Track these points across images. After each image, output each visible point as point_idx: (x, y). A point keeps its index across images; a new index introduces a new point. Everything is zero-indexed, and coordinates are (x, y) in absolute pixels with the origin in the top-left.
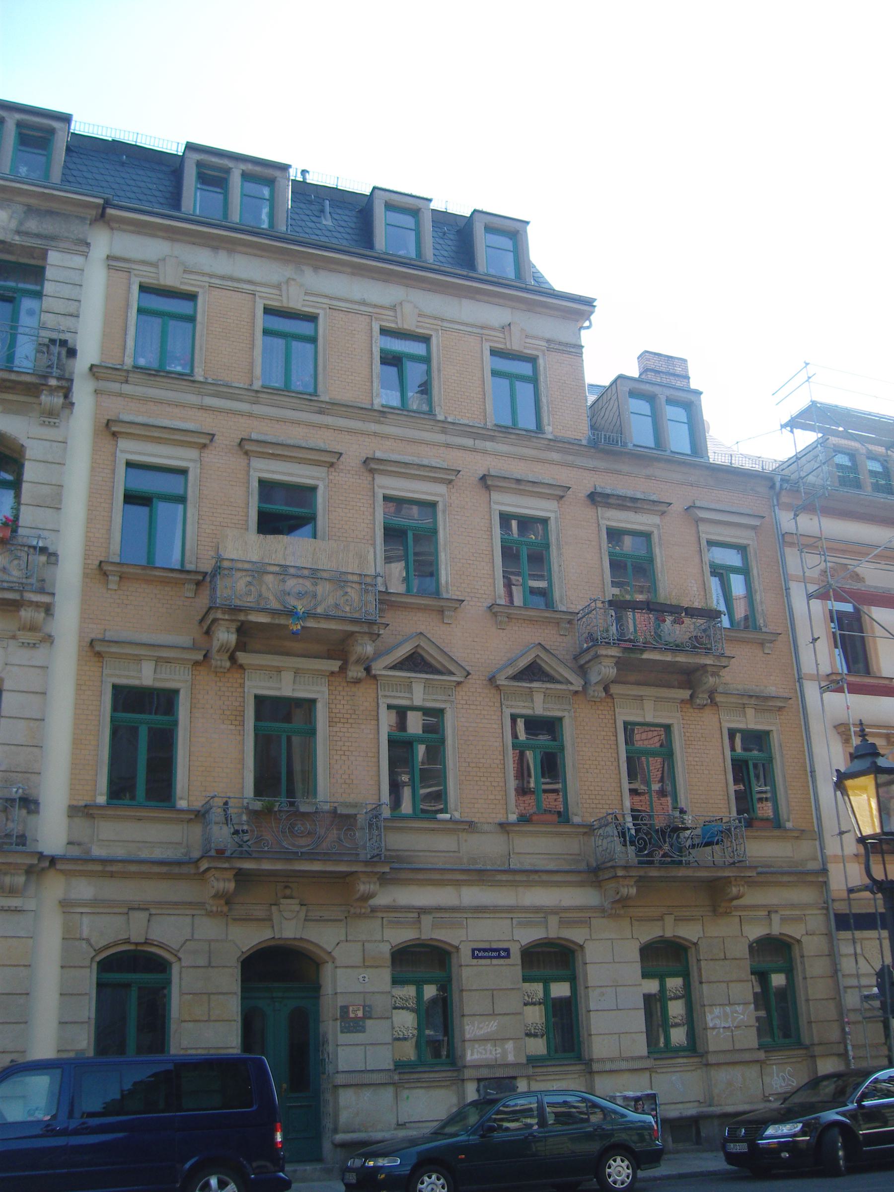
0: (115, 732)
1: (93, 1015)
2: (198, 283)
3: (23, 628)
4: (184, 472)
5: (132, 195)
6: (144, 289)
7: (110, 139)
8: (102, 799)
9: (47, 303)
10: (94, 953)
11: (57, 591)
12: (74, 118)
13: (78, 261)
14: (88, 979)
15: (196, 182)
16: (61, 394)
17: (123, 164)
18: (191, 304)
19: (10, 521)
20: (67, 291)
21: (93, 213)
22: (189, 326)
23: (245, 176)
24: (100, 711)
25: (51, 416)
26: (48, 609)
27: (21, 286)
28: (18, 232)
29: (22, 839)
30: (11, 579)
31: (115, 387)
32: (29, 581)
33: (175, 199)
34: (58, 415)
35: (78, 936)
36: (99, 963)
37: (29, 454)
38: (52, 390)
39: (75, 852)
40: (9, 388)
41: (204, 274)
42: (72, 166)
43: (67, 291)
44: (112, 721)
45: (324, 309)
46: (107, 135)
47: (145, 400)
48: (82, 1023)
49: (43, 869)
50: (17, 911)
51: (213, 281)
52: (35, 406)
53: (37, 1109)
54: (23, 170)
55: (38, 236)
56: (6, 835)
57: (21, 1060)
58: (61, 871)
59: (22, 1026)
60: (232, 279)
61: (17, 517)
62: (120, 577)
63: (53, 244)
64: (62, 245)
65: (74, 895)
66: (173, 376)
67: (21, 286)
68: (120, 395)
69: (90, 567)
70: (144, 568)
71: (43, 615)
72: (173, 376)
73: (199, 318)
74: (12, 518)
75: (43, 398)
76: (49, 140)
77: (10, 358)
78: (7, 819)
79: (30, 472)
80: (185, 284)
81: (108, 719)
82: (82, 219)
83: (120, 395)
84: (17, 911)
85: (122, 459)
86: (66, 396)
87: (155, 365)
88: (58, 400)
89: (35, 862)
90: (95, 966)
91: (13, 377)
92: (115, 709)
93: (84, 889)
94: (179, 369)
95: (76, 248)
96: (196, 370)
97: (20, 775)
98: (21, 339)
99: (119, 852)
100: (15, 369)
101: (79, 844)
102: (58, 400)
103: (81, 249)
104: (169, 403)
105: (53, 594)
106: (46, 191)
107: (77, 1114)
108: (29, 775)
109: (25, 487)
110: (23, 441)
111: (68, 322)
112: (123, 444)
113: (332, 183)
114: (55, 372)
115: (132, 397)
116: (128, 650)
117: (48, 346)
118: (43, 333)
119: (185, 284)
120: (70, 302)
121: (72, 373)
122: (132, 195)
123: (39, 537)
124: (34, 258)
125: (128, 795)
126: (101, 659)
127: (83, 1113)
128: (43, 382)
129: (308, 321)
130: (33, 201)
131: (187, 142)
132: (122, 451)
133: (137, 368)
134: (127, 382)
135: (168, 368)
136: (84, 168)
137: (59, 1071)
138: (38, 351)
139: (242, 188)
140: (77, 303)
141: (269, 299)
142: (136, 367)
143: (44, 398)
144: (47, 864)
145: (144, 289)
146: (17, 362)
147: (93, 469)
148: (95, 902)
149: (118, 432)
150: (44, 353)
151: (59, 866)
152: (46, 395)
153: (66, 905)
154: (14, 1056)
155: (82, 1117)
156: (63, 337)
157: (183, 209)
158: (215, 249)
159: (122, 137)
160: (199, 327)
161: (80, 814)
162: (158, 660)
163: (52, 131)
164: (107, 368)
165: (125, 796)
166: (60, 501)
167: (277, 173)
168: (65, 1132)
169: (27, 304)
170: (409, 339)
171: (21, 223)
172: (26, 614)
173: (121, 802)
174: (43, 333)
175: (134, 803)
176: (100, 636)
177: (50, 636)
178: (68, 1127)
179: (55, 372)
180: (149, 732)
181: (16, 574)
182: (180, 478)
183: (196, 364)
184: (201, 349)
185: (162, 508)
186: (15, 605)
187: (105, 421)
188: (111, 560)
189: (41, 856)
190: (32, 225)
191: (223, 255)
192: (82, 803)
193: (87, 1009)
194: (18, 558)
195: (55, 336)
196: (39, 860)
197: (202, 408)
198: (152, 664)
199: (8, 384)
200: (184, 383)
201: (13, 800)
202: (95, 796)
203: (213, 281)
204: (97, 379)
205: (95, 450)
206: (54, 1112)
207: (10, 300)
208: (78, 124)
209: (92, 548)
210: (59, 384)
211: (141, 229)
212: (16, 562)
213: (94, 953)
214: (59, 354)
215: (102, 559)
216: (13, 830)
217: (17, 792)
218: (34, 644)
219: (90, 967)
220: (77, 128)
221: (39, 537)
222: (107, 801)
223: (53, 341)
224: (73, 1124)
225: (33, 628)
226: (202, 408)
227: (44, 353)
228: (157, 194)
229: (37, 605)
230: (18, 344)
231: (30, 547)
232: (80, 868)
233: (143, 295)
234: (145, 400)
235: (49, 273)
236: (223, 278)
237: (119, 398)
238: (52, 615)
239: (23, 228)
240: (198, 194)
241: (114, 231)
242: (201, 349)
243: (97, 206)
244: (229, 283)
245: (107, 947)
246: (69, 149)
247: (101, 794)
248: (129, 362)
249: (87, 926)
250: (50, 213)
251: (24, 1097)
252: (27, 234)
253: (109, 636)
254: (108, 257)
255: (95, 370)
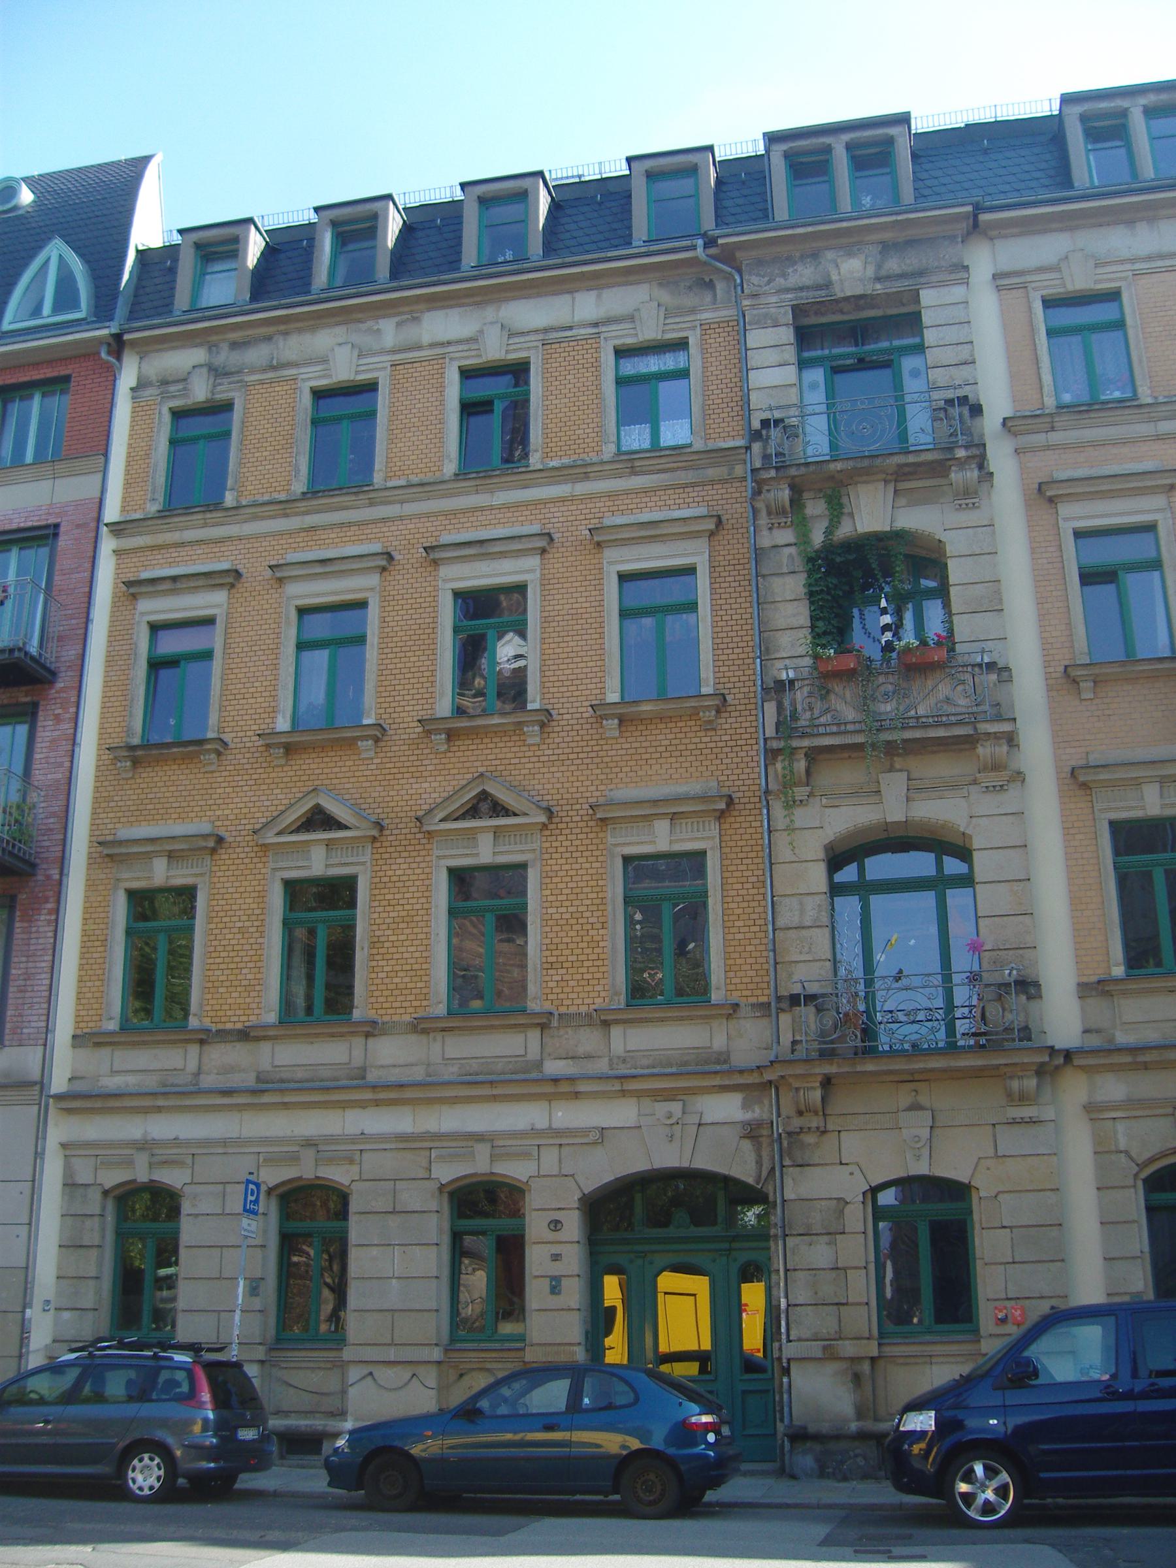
0: (1123, 880)
1: (1147, 1249)
2: (1118, 275)
3: (983, 769)
4: (1150, 528)
5: (1007, 188)
6: (1048, 303)
7: (962, 125)
8: (1119, 971)
9: (932, 356)
10: (1136, 1169)
11: (1017, 716)
12: (913, 116)
13: (958, 292)
14: (1134, 1203)
15: (1086, 144)
16: (973, 466)
17: (986, 152)
18: (1115, 305)
19: (945, 638)
20: (951, 334)
21: (964, 226)
22: (1117, 335)
23: (1150, 113)
24: (1098, 858)
25: (968, 497)
26: (1011, 739)
27: (897, 343)
28: (878, 279)
29: (1026, 1033)
30: (959, 710)
31: (1040, 439)
32: (980, 708)
33: (1063, 175)
34: (976, 493)
35: (1113, 1148)
36: (1145, 1181)
37: (949, 550)
38: (962, 463)
39: (1094, 1041)
40: (909, 473)
41: (1122, 262)
42: (924, 175)
43: (951, 334)
44: (1115, 868)
45: (1125, 279)
46: (957, 121)
47: (1080, 446)
48: (1134, 1258)
49: (1057, 1068)
50: (1032, 1122)
51: (1137, 266)
52: (945, 488)
53: (1091, 1367)
54: (867, 201)
55: (902, 276)
56: (1006, 1029)
57: (1062, 1305)
58: (1080, 1067)
59: (1059, 1264)
60: (1161, 256)
61: (951, 632)
62: (1095, 682)
63: (923, 280)
64: (934, 278)
65: (1101, 1096)
66: (1110, 406)
67: (897, 343)
68: (1048, 447)
69: (1054, 675)
70: (1122, 663)
71: (1005, 748)
72: (1110, 406)
73: (1129, 321)
74: (944, 634)
75: (953, 475)
76: (889, 153)
77: (903, 436)
78: (1004, 1010)
79: (956, 572)
80: (1100, 281)
81: (1111, 867)
82: (952, 238)
83: (1048, 447)
84: (1032, 1122)
85: (1067, 529)
86: (981, 467)
87: (1086, 398)
88: (973, 474)
89: (1047, 1059)
90: (1140, 1184)
91: (911, 459)
92: (1117, 852)
93: (1113, 1088)
94: (1117, 394)
95: (953, 276)
96: (1140, 390)
97: (1011, 952)
98: (910, 410)
99: (1151, 1035)
100: (911, 449)
101: (1098, 1031)
102: (973, 474)
103: (958, 276)
104: (1115, 443)
105: (1015, 719)
106: (900, 218)
107: (1143, 1372)
108: (1021, 952)
109: (953, 591)
110: (940, 535)
111: (963, 373)
112: (1065, 510)
113: (988, 116)
114: (961, 439)
115: (1064, 447)
116: (1121, 774)
117: (946, 410)
118: (936, 395)
119: (1100, 281)
120: (960, 347)
121: (982, 435)
122: (1007, 188)
123: (983, 651)
124: (903, 305)
125: (1151, 961)
126: (1088, 792)
127: (1151, 1372)
128: (949, 456)
129: (1110, 301)
130: (887, 236)
131: (764, 134)
132: (1066, 519)
133: (1063, 407)
134: (1053, 429)
135: (1103, 398)
136: (939, 173)
137: (1112, 1319)
138: (934, 420)
139: (1148, 128)
140: (969, 346)
141: (1046, 287)
142: (1060, 407)
143: (955, 476)
144: (1061, 1060)
145: (1048, 303)
146: (911, 440)
147: (1033, 551)
148: (1130, 1103)
149: (1056, 496)
150: (941, 419)
151: (1076, 1062)
152: (956, 472)
153: (1092, 1110)
154: (1054, 1302)
155: (1150, 1376)
156: (960, 393)
157: (1076, 185)
158: (1130, 223)
159: (976, 118)
160: (1131, 332)
161: (1094, 993)
162: (674, 817)
163: (890, 141)
164: (1025, 417)
165: (1148, 962)
166: (1001, 601)
167: (893, 131)
168: (1129, 1396)
169: (908, 363)
170: (635, 356)
171: (879, 267)
172: (984, 751)
173: (1142, 971)
174: (936, 395)
175: (313, 1019)
176: (1082, 762)
177: (1019, 773)
178: (1132, 1390)
179: (961, 439)
180: (1167, 878)
181: (963, 702)
182: (1148, 537)
183: (1138, 383)
184: (1140, 361)
185: (1131, 580)
186: (969, 742)
187: (1036, 486)
188: (1078, 662)
189: (1052, 1050)
190: (893, 265)
191: (1142, 228)
192: (1094, 979)
193: (1138, 1240)
194: (963, 682)
195: (950, 394)
196: (1050, 1055)
197: (1159, 438)
198: (164, 860)
199: (907, 469)
200: (1127, 411)
201: (1008, 985)
202: (1109, 968)
203: (1137, 266)
204: (1015, 435)
205: (1031, 526)
206: (1113, 1370)
207: (887, 365)
208: (919, 120)
209: (1051, 652)
210: (969, 453)
211: (1028, 227)
212: (960, 688)
213: (1136, 1169)
214: (961, 415)
215: (1067, 663)
216: (1012, 1022)
217: (1010, 974)
218: (1001, 786)
219: (1135, 1186)
220: (919, 126)
221: (983, 651)
222: (1126, 971)
223: (950, 402)
224: (1139, 1386)
225: (996, 766)
226: (1159, 438)
227: (941, 419)
228: (1038, 174)
229: (996, 736)
230: (909, 416)
231: (973, 666)
232: (1102, 1061)
233: (1050, 311)
234: (1080, 446)
235: (927, 318)
236: (1150, 258)
237: (1048, 452)
238: (1018, 746)
239: (883, 273)
240: (1091, 158)
241: (995, 241)
242: (1140, 361)
243: (965, 216)
244: (1160, 263)
245: (1152, 1160)
246: (914, 156)
247: (1117, 965)
248: (1050, 402)
249: (1121, 1135)
250: (910, 243)
251: (1073, 1353)
252: (888, 278)
253: (1094, 759)
254: (995, 277)
255: (1009, 424)
